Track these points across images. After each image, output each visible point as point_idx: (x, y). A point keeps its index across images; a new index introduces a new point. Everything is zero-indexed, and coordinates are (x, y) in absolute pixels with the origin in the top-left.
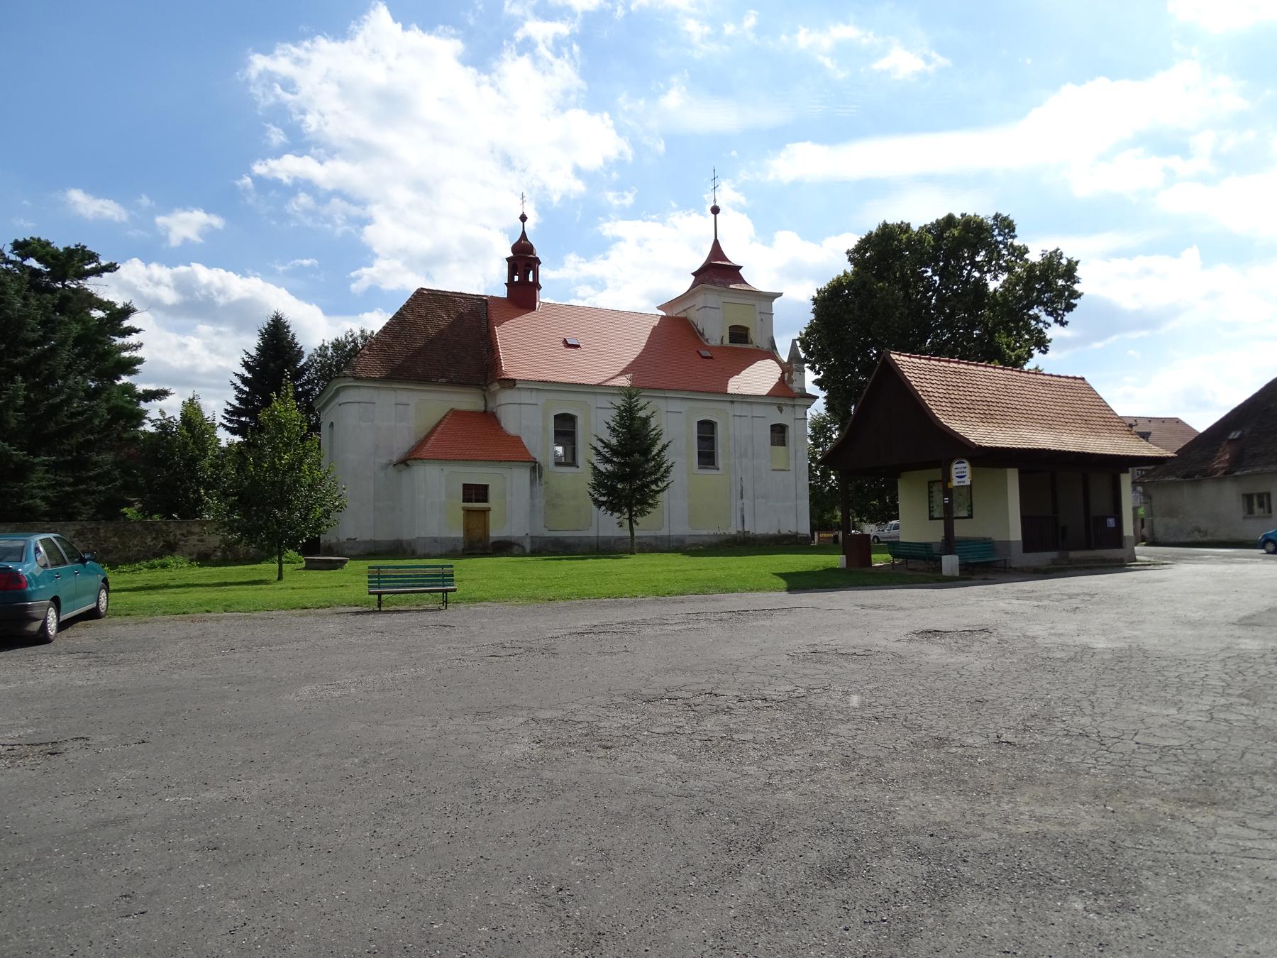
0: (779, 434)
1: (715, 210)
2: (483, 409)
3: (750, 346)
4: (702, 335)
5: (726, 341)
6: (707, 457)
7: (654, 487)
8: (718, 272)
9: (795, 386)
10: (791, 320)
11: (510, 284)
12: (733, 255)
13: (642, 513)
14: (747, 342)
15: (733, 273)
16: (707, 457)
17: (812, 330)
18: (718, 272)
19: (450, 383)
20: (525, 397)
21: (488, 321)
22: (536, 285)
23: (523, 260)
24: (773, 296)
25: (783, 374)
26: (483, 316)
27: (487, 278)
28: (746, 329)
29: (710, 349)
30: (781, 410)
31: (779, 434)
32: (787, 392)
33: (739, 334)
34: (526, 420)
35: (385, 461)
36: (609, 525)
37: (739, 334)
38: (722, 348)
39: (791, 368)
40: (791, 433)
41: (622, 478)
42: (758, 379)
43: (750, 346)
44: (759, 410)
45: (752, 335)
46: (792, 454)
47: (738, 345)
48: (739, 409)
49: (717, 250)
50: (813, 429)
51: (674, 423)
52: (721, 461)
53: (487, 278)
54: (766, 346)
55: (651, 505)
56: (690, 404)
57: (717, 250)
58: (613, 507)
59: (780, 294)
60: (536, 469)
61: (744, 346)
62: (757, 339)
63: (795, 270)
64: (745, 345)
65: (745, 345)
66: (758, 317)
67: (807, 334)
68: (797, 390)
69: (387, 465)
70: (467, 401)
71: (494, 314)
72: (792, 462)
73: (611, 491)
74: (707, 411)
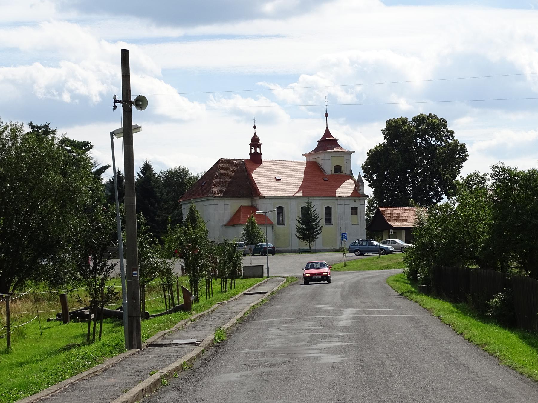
0: (354, 210)
1: (327, 115)
2: (251, 205)
3: (342, 174)
4: (324, 170)
5: (333, 172)
6: (328, 221)
7: (317, 233)
8: (327, 143)
9: (360, 192)
10: (358, 161)
11: (251, 154)
12: (335, 134)
13: (313, 241)
14: (341, 172)
15: (335, 143)
16: (328, 221)
17: (367, 164)
18: (327, 143)
19: (242, 197)
20: (268, 201)
21: (247, 170)
22: (260, 154)
23: (255, 142)
24: (351, 153)
25: (355, 186)
26: (244, 167)
27: (244, 154)
28: (341, 167)
29: (327, 176)
30: (355, 202)
31: (354, 210)
32: (358, 194)
33: (338, 169)
34: (266, 209)
35: (222, 224)
36: (304, 244)
37: (338, 169)
38: (331, 176)
39: (359, 184)
40: (359, 210)
41: (307, 230)
42: (346, 189)
43: (342, 174)
44: (347, 202)
45: (343, 169)
46: (359, 218)
47: (337, 174)
48: (340, 202)
49: (327, 133)
50: (368, 203)
51: (318, 208)
52: (333, 222)
53: (243, 153)
54: (348, 173)
55: (317, 239)
56: (321, 201)
57: (327, 133)
58: (304, 239)
59: (354, 152)
60: (272, 225)
61: (340, 174)
62: (345, 171)
63: (361, 141)
64: (341, 174)
65: (341, 174)
66: (345, 162)
67: (365, 165)
68: (361, 194)
69: (223, 226)
70: (246, 202)
71: (249, 167)
72: (359, 222)
73: (303, 234)
74: (328, 203)
